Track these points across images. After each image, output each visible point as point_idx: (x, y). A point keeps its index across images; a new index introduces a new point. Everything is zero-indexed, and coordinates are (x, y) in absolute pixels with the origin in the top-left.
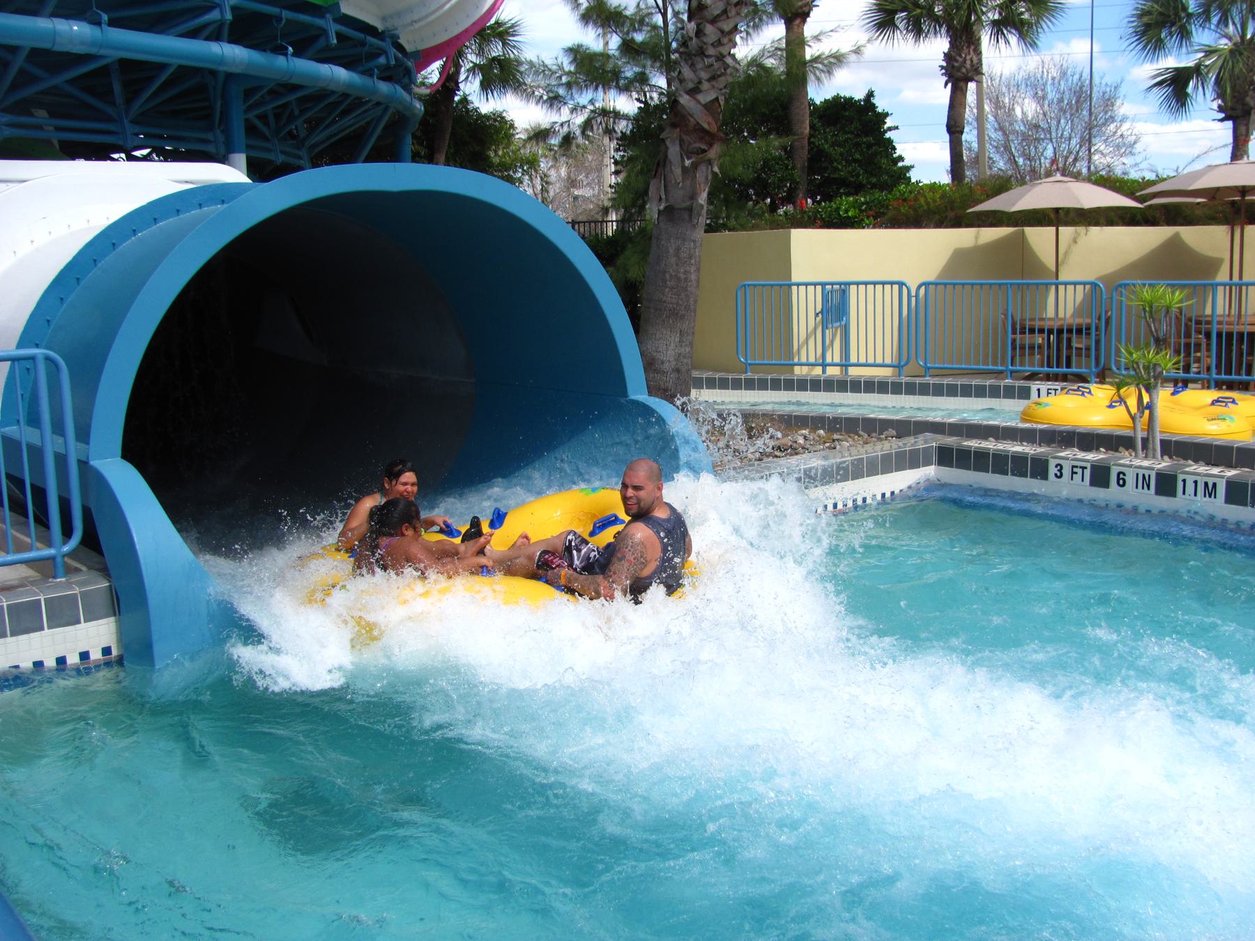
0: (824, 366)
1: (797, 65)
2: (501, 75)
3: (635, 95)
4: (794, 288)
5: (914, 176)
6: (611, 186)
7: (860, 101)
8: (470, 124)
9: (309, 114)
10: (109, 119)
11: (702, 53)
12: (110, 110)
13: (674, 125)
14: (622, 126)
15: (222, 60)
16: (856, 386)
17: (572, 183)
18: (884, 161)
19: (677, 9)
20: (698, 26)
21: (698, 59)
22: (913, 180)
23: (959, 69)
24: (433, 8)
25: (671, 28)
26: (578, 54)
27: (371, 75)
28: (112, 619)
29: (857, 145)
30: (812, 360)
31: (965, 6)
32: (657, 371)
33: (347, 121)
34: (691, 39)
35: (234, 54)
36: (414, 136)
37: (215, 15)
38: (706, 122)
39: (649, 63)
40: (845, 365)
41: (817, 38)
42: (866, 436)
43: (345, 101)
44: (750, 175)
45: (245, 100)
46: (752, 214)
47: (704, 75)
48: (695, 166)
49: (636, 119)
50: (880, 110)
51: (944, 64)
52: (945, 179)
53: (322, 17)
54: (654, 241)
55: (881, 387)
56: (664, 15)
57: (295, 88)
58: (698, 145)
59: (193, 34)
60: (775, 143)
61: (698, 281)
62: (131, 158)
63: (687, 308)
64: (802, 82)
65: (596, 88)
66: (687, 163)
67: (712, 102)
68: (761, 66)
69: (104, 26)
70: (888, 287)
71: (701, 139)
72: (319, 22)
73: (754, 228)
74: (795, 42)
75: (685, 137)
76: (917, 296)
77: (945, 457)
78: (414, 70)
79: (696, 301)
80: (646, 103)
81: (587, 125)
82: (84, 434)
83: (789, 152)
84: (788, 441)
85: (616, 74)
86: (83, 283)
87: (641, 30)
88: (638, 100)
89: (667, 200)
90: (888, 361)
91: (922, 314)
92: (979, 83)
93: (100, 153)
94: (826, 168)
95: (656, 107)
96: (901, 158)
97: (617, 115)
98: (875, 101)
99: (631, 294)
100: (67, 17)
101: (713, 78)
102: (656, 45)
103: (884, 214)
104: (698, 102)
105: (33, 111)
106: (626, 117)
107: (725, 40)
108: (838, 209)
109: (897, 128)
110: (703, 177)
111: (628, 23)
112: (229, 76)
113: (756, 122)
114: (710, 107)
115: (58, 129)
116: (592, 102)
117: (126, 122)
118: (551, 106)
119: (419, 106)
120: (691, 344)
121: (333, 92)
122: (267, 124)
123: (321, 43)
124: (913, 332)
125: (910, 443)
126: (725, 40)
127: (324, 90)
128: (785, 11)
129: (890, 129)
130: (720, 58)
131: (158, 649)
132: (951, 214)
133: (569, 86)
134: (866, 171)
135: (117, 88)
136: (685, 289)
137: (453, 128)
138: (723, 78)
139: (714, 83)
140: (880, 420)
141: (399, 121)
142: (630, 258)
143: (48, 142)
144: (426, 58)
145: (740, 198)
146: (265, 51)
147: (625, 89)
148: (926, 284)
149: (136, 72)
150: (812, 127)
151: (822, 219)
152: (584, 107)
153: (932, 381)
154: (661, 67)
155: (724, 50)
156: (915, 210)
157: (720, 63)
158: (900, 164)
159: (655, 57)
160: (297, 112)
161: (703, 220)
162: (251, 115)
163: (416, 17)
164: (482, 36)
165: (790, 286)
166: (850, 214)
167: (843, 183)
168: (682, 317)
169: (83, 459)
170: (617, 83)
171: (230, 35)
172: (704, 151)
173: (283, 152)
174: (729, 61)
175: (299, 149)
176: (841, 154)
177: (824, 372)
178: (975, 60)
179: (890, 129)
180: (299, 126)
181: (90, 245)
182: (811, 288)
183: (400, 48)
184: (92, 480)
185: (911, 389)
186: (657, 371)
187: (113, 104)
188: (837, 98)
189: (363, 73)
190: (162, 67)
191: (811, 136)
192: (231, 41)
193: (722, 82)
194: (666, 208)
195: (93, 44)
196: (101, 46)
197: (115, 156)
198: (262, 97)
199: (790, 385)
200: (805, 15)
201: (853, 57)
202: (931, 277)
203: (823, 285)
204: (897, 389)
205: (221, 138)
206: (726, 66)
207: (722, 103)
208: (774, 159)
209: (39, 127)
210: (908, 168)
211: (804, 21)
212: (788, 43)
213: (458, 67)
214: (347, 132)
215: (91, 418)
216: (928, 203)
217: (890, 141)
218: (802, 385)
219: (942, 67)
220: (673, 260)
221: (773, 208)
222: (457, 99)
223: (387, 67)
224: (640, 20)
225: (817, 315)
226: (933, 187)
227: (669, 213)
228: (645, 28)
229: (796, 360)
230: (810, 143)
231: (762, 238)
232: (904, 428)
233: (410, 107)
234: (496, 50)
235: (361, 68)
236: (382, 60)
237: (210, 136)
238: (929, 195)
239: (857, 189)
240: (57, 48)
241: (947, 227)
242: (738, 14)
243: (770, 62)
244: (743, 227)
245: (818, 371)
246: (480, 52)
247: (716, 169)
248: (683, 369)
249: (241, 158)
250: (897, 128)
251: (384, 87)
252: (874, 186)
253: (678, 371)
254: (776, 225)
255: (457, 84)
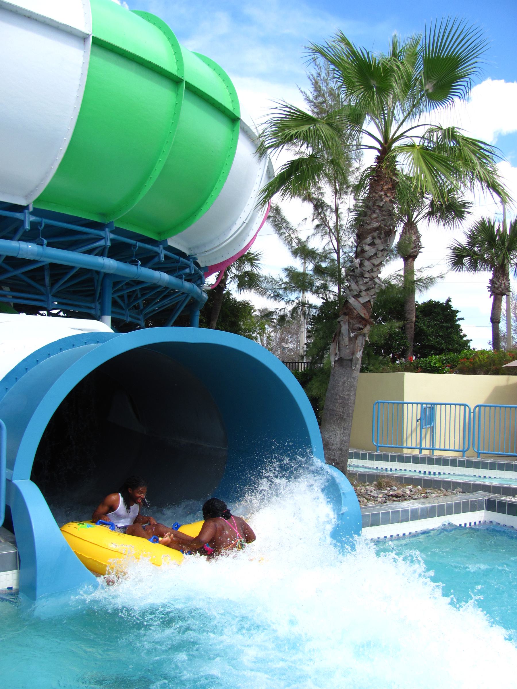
0: (421, 449)
1: (410, 284)
2: (249, 281)
3: (321, 296)
4: (405, 405)
5: (472, 345)
6: (305, 344)
7: (443, 304)
8: (230, 306)
9: (147, 296)
10: (42, 294)
11: (362, 276)
12: (42, 289)
13: (345, 314)
14: (314, 312)
15: (103, 266)
16: (438, 461)
17: (282, 340)
18: (456, 336)
19: (345, 250)
20: (361, 261)
21: (360, 279)
22: (471, 348)
23: (497, 289)
24: (215, 246)
25: (342, 261)
26: (291, 272)
27: (181, 278)
28: (15, 571)
29: (441, 327)
30: (414, 446)
31: (502, 255)
32: (330, 449)
33: (165, 302)
34: (357, 268)
35: (110, 264)
36: (201, 311)
37: (102, 243)
38: (364, 313)
39: (329, 279)
40: (432, 449)
41: (420, 271)
42: (445, 491)
43: (166, 292)
44: (382, 341)
45: (113, 288)
46: (381, 363)
47: (363, 288)
48: (356, 337)
49: (321, 309)
50: (454, 309)
51: (490, 285)
52: (489, 348)
53: (158, 246)
54: (331, 377)
55: (452, 463)
56: (338, 254)
57: (139, 283)
58: (358, 325)
59: (89, 252)
60: (396, 324)
61: (354, 400)
62: (49, 314)
63: (348, 415)
64: (413, 292)
65: (300, 292)
66: (352, 335)
67: (367, 302)
68: (389, 283)
69: (45, 246)
70: (458, 407)
71: (360, 322)
72: (156, 249)
73: (383, 371)
74: (409, 270)
75: (351, 321)
76: (474, 412)
77: (491, 506)
78: (203, 276)
79: (353, 411)
80: (326, 300)
81: (295, 310)
82: (11, 465)
83: (403, 328)
84: (400, 492)
85: (311, 284)
86: (19, 381)
87: (325, 261)
88: (322, 298)
89: (340, 355)
90: (457, 448)
91: (474, 421)
92: (508, 296)
93: (33, 311)
94: (424, 340)
95: (332, 302)
96: (465, 336)
97: (311, 306)
98: (451, 304)
99: (315, 402)
100: (26, 241)
101: (368, 290)
102: (333, 270)
103: (456, 366)
104: (359, 302)
105: (3, 287)
106: (315, 307)
107: (375, 270)
108: (430, 362)
109: (463, 319)
110: (360, 343)
111: (318, 257)
112: (106, 275)
113: (386, 313)
114: (365, 305)
115: (14, 297)
116: (297, 298)
117: (50, 295)
118: (275, 299)
119: (205, 296)
120: (349, 435)
121: (160, 286)
122: (123, 300)
123: (156, 260)
124: (476, 436)
125: (470, 497)
126: (375, 270)
127: (154, 284)
128: (403, 254)
129: (459, 319)
130: (372, 279)
131: (39, 591)
132: (493, 368)
133: (285, 289)
134: (446, 342)
135: (47, 280)
136: (347, 404)
137: (222, 308)
138: (373, 290)
139: (368, 292)
140: (453, 482)
141: (194, 303)
142: (314, 384)
143: (8, 304)
144: (210, 270)
145: (376, 353)
146: (126, 262)
147: (316, 292)
148: (479, 406)
149: (57, 270)
150: (417, 317)
151: (421, 367)
152: (293, 301)
153: (481, 460)
154: (335, 281)
155: (374, 275)
156: (473, 364)
157: (372, 282)
158: (464, 339)
159: (332, 275)
160: (139, 296)
161: (359, 367)
162: (115, 296)
163: (207, 249)
164: (240, 260)
165: (403, 404)
166: (437, 365)
167: (432, 348)
168: (345, 420)
169: (9, 479)
170: (311, 289)
171: (109, 253)
172: (361, 329)
173: (130, 316)
174: (377, 280)
175: (139, 315)
176: (432, 332)
177: (420, 452)
178: (507, 285)
179: (459, 319)
180: (141, 302)
181: (25, 360)
182: (415, 406)
183: (197, 264)
184: (12, 490)
185: (469, 465)
186: (330, 449)
187: (44, 285)
188: (430, 302)
189: (177, 277)
190: (71, 268)
191: (416, 321)
192: (109, 257)
193: (372, 292)
194: (339, 359)
195: (38, 254)
196: (42, 256)
197: (41, 312)
198: (122, 286)
199: (401, 459)
200: (414, 257)
201: (439, 280)
202: (481, 403)
203: (422, 404)
204: (461, 464)
205: (99, 307)
206: (375, 284)
207: (372, 303)
208: (395, 333)
209: (5, 296)
210: (469, 341)
211: (414, 260)
212: (405, 272)
213: (226, 276)
214: (164, 308)
215: (16, 456)
216: (480, 361)
217: (459, 326)
218: (408, 459)
219: (489, 287)
220: (341, 388)
221: (394, 360)
222: (224, 292)
223: (190, 274)
224: (324, 256)
225: (418, 421)
226: (483, 352)
227: (340, 361)
228: (327, 260)
229: (405, 445)
230: (415, 325)
231: (389, 377)
232: (468, 488)
233: (200, 296)
234: (247, 268)
235: (176, 274)
236: (187, 271)
237: (93, 305)
238: (481, 357)
239: (441, 351)
240: (19, 256)
241: (491, 375)
242: (383, 256)
243: (394, 282)
244: (377, 370)
245: (417, 452)
246: (239, 268)
247: (367, 339)
248: (344, 449)
249: (108, 318)
250: (463, 319)
251: (187, 285)
252: (450, 350)
253: (341, 449)
254: (396, 370)
255: (225, 284)
